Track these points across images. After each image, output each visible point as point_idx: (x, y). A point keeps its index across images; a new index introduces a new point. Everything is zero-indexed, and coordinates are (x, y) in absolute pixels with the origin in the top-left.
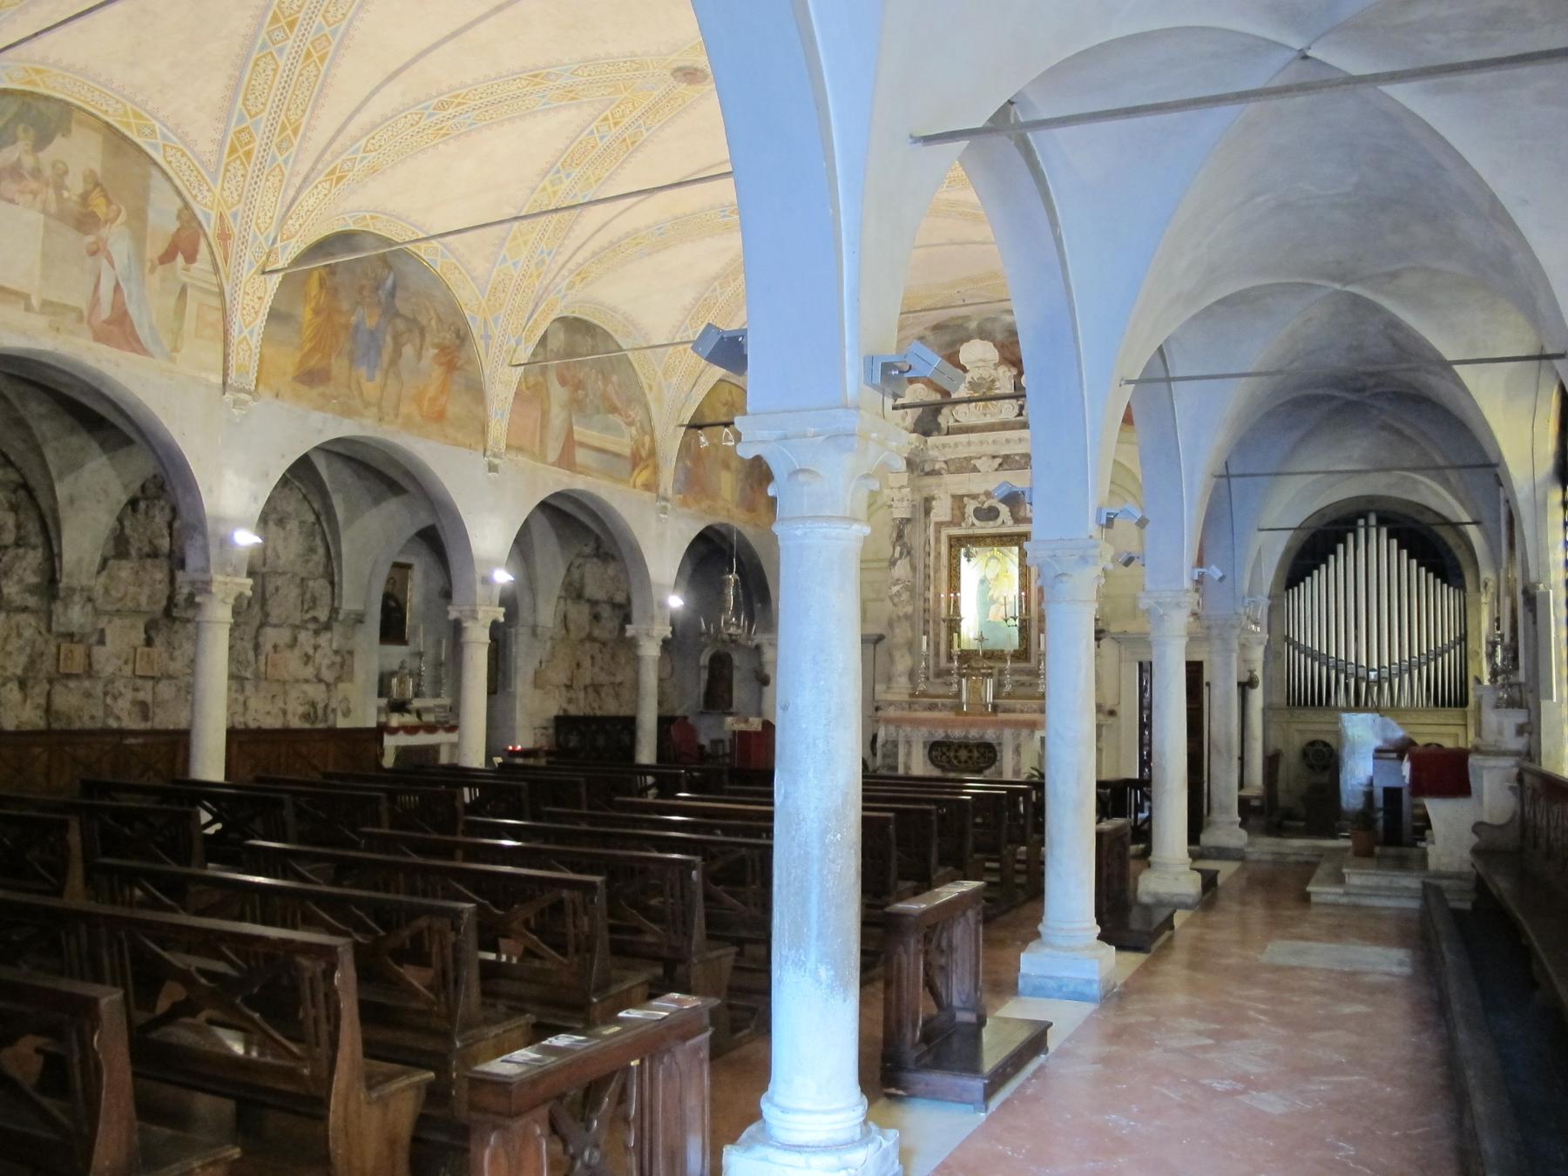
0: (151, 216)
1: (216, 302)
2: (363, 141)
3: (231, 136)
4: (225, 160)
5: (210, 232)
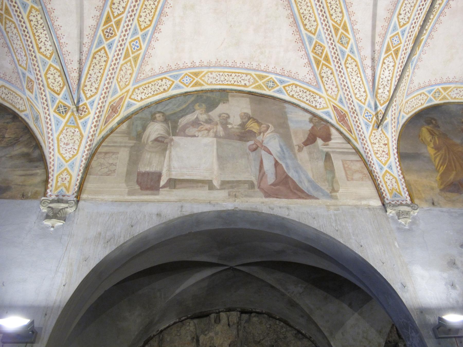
0: (291, 125)
1: (357, 158)
2: (395, 19)
3: (311, 55)
4: (317, 72)
5: (334, 122)
